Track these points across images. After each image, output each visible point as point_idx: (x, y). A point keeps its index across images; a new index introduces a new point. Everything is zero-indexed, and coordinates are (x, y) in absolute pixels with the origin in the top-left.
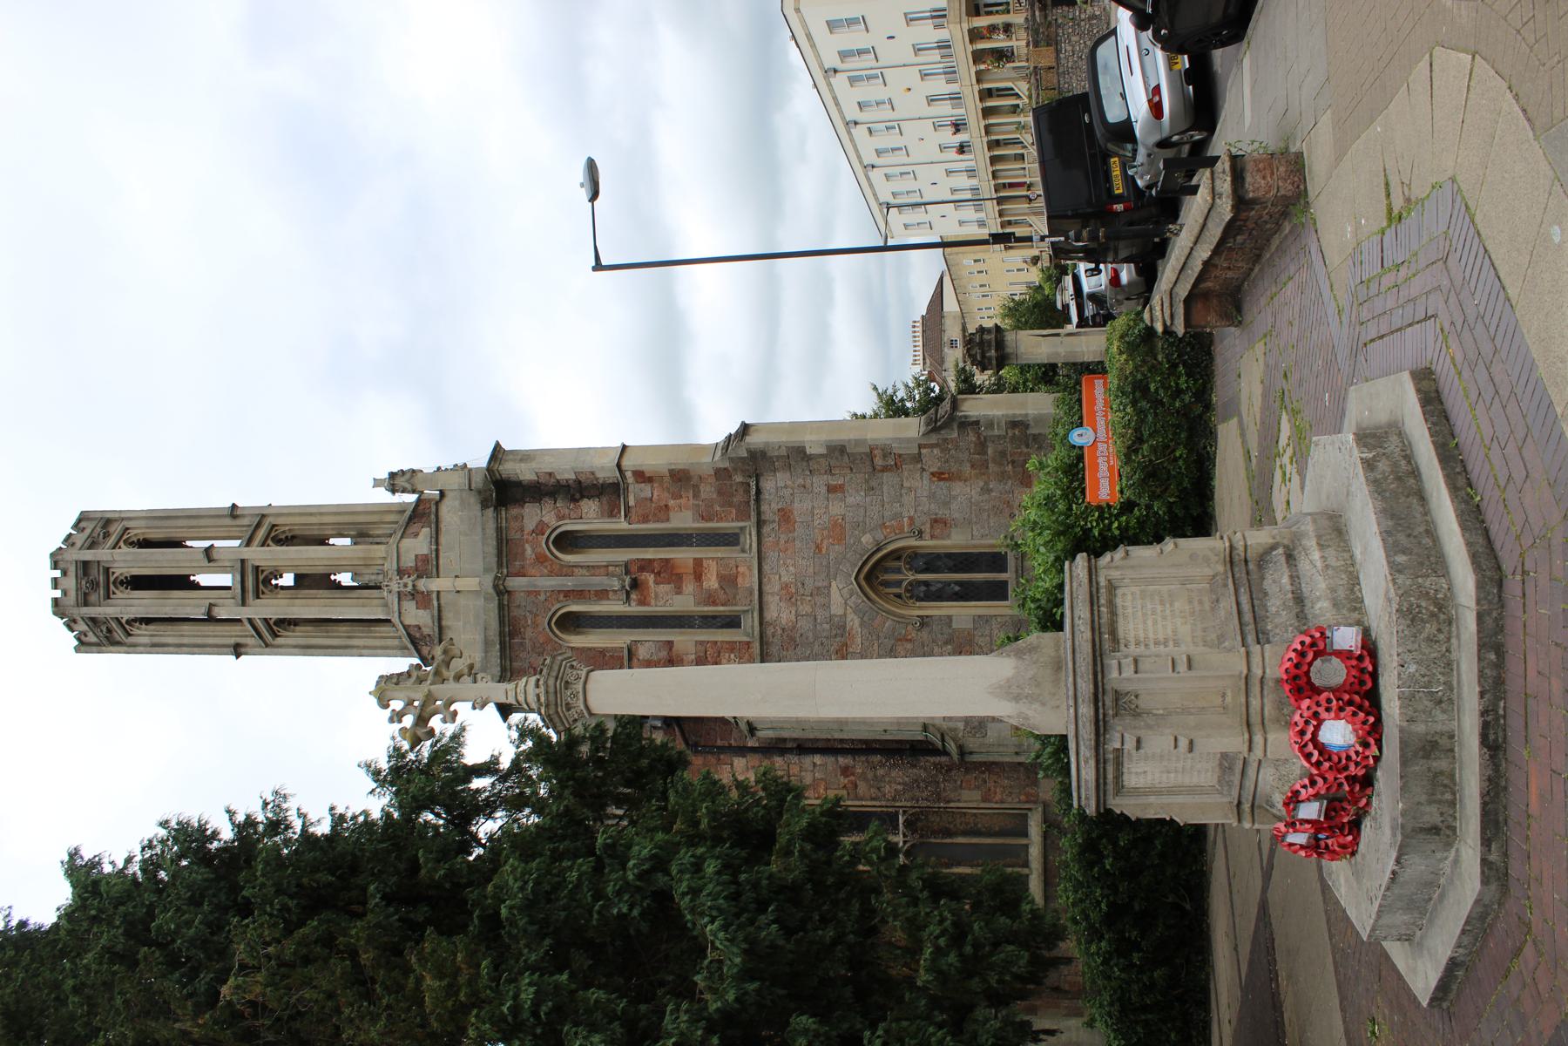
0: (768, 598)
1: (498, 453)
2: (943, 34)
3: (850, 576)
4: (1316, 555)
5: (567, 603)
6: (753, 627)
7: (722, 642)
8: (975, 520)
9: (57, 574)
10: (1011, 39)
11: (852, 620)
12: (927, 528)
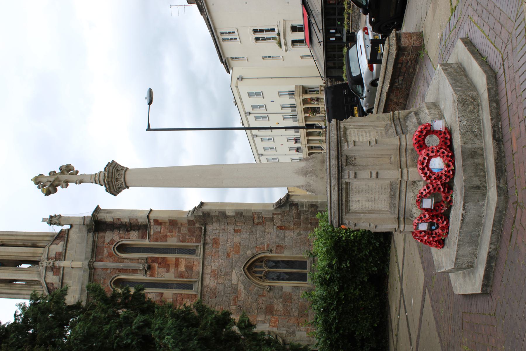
0: (206, 276)
1: (97, 210)
2: (293, 102)
3: (241, 267)
4: (427, 111)
5: (119, 274)
6: (198, 288)
7: (184, 294)
8: (294, 246)
10: (319, 104)
11: (240, 286)
12: (274, 249)
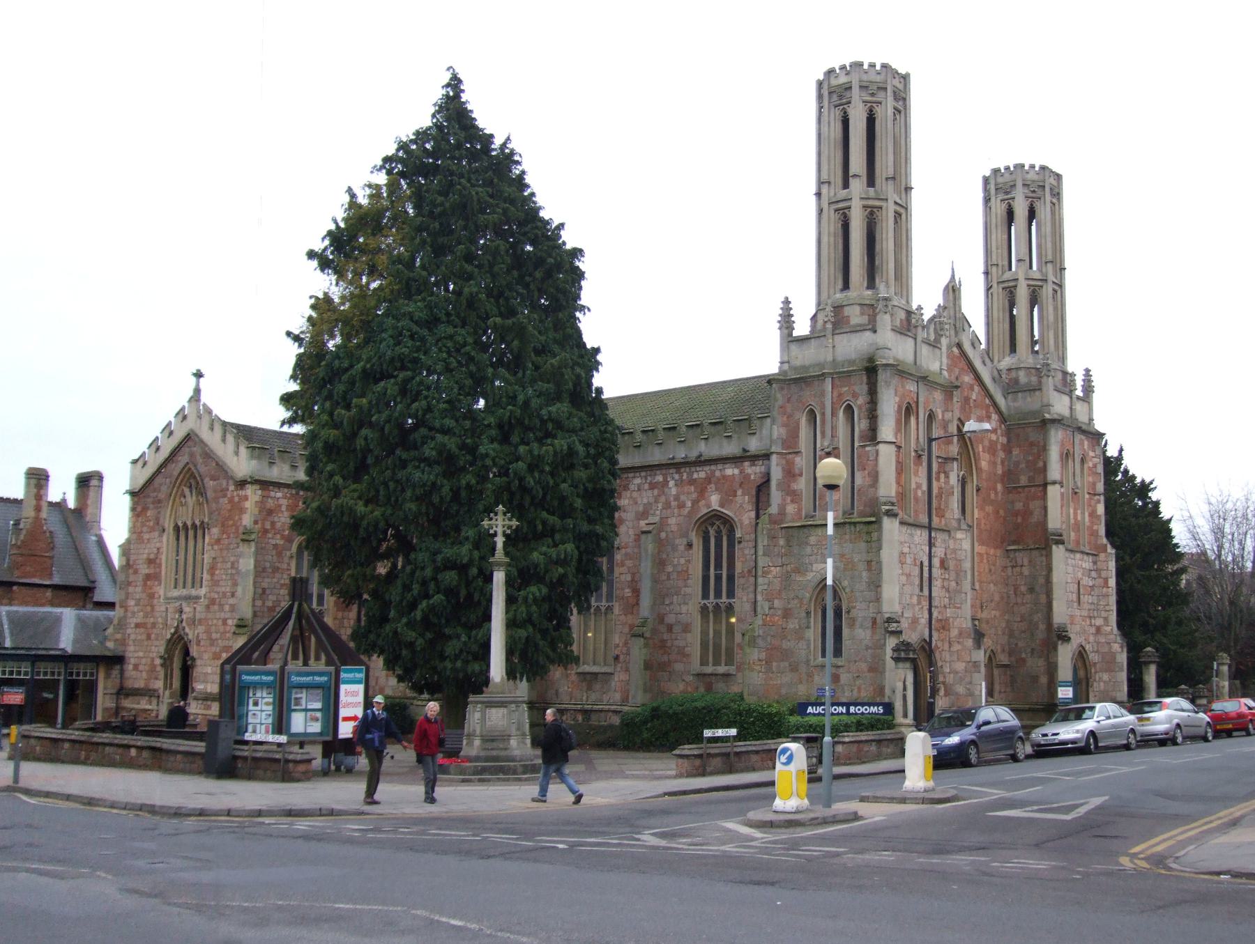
9: (878, 68)
